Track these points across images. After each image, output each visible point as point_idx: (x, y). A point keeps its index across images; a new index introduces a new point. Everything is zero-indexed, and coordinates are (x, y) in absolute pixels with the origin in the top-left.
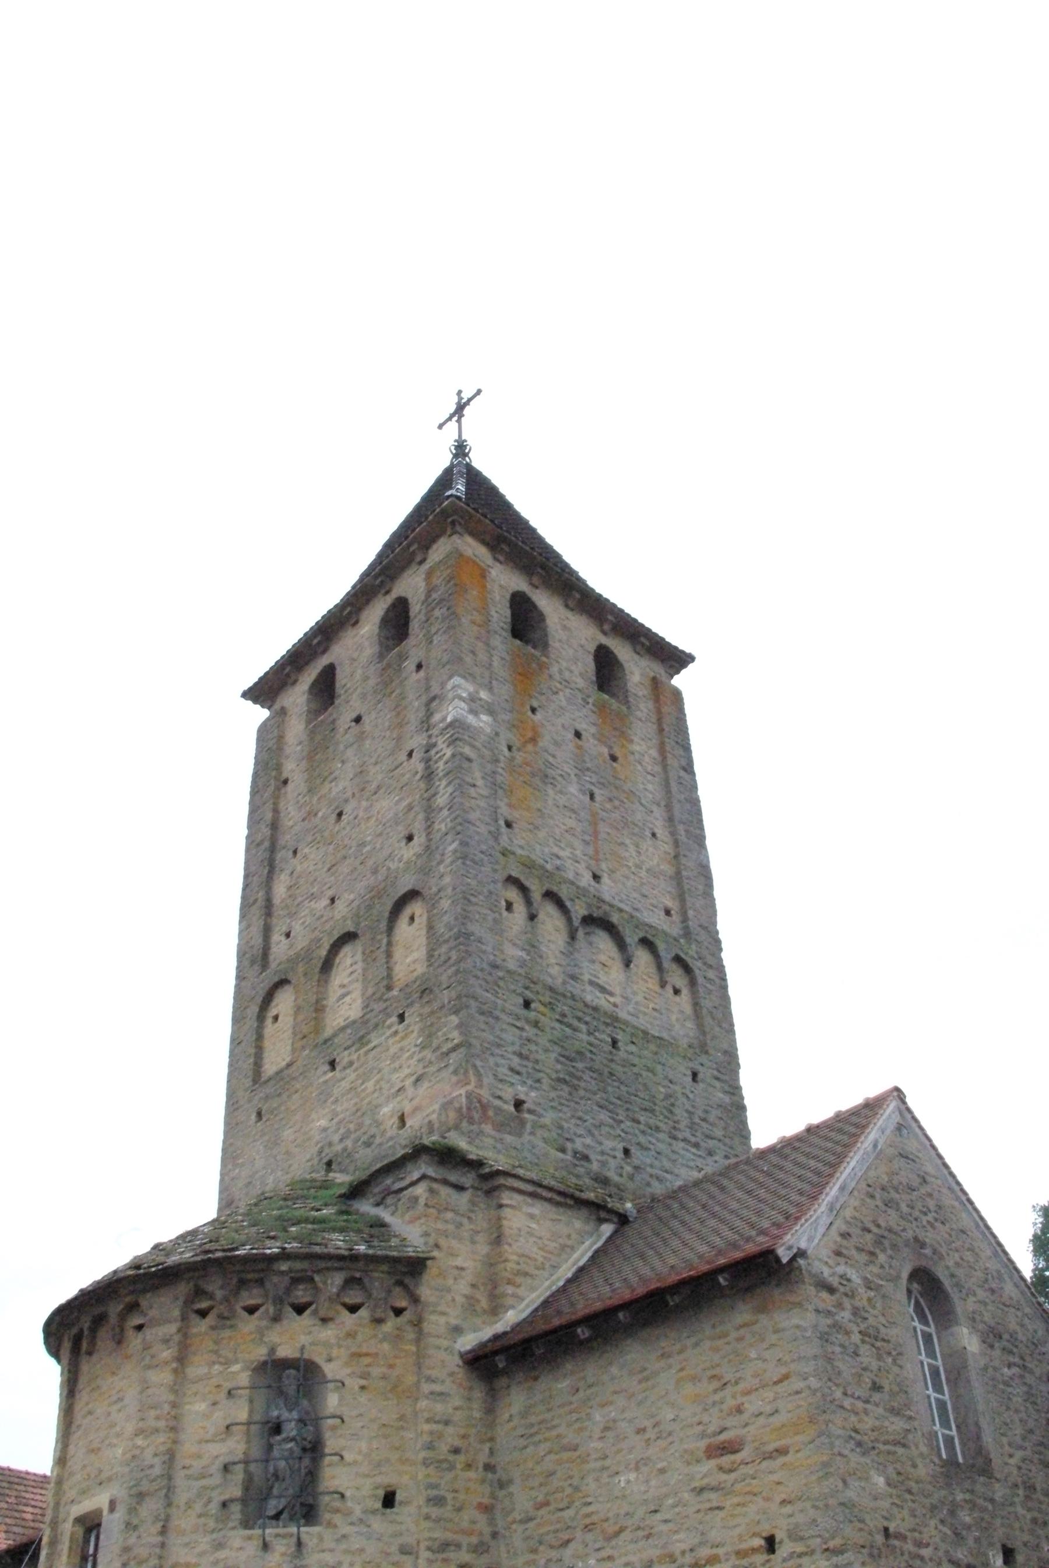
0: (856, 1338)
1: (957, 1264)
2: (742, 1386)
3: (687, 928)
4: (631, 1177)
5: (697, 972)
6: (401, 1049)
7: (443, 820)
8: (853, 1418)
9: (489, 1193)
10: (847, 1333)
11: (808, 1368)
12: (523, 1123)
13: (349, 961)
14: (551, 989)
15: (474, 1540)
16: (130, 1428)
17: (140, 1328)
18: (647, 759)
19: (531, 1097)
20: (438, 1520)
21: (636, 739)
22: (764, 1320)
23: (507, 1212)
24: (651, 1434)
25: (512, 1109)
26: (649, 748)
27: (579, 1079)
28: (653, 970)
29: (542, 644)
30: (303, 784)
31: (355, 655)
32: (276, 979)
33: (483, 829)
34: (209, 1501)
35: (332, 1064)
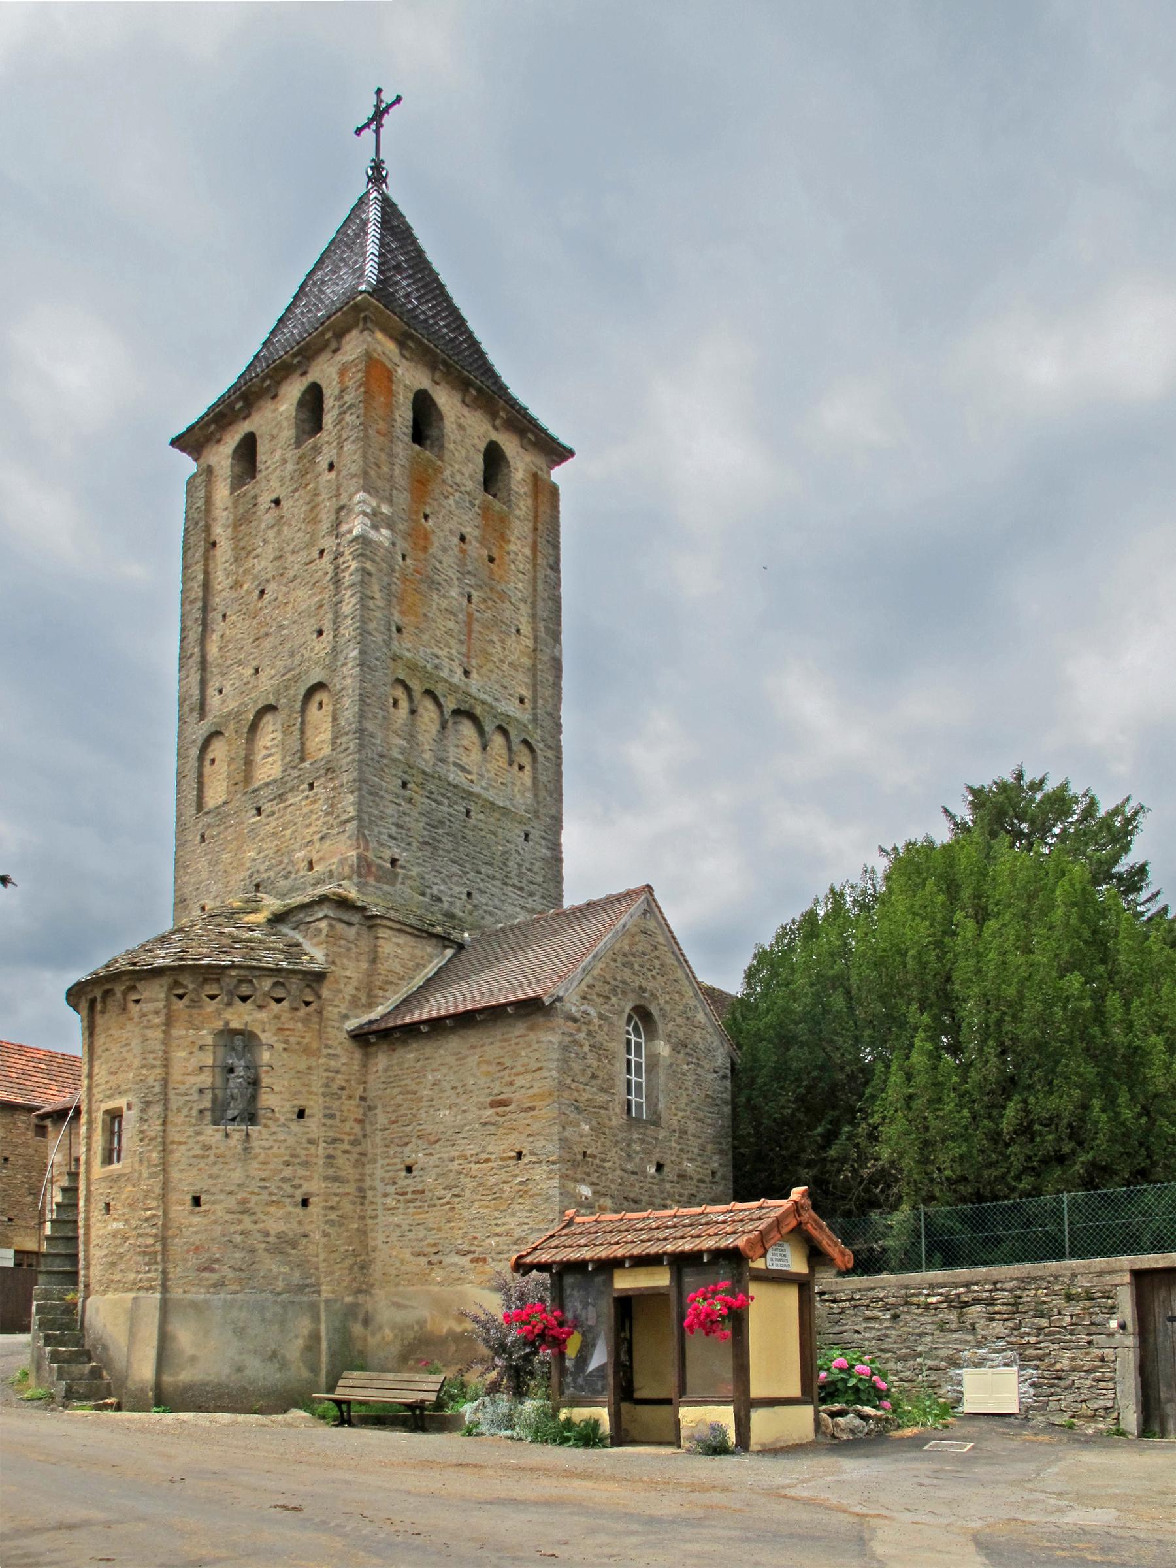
0: (586, 1048)
1: (667, 1002)
2: (514, 1071)
3: (535, 715)
4: (471, 913)
5: (539, 752)
6: (311, 812)
7: (347, 628)
8: (576, 1094)
9: (370, 927)
10: (581, 1046)
11: (554, 1065)
12: (396, 875)
13: (271, 728)
14: (424, 772)
15: (352, 1138)
16: (137, 1062)
17: (137, 1001)
18: (520, 557)
19: (403, 856)
20: (331, 1126)
21: (513, 539)
22: (532, 1036)
23: (381, 942)
24: (460, 1090)
25: (389, 865)
26: (523, 546)
27: (439, 841)
28: (504, 752)
29: (439, 445)
30: (229, 552)
31: (275, 432)
32: (213, 729)
33: (379, 638)
34: (191, 1109)
35: (259, 811)
